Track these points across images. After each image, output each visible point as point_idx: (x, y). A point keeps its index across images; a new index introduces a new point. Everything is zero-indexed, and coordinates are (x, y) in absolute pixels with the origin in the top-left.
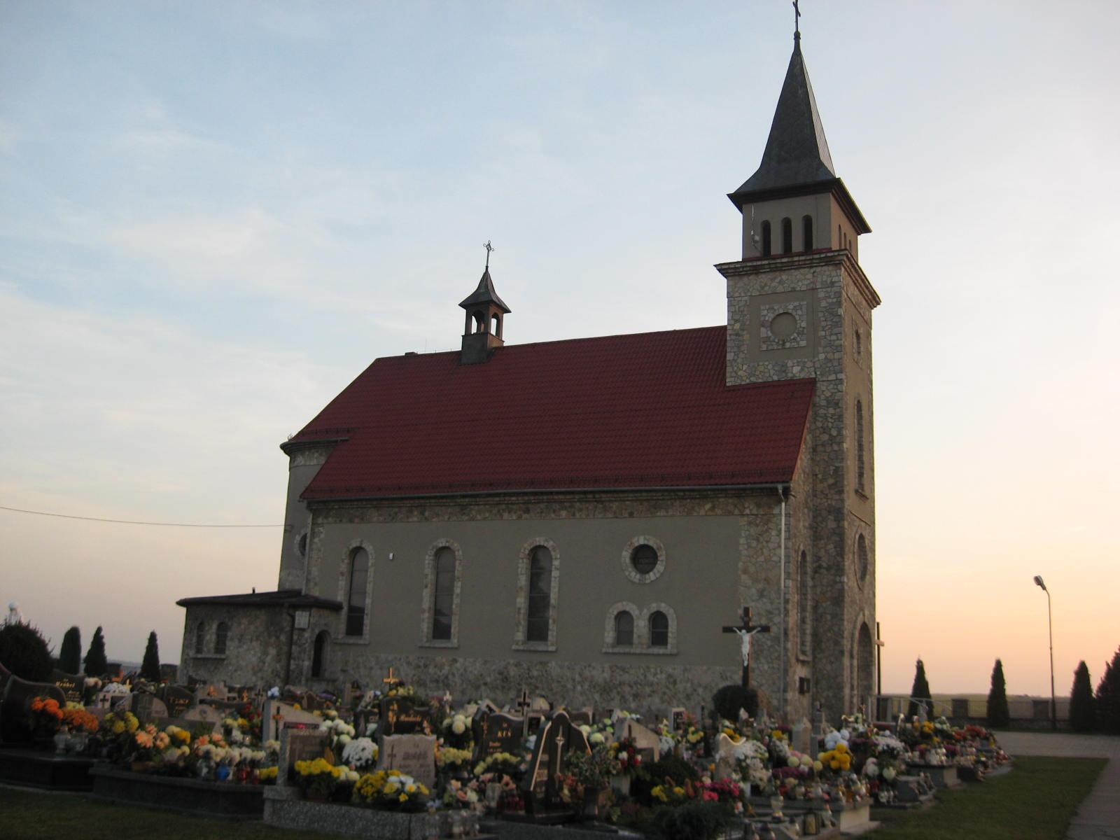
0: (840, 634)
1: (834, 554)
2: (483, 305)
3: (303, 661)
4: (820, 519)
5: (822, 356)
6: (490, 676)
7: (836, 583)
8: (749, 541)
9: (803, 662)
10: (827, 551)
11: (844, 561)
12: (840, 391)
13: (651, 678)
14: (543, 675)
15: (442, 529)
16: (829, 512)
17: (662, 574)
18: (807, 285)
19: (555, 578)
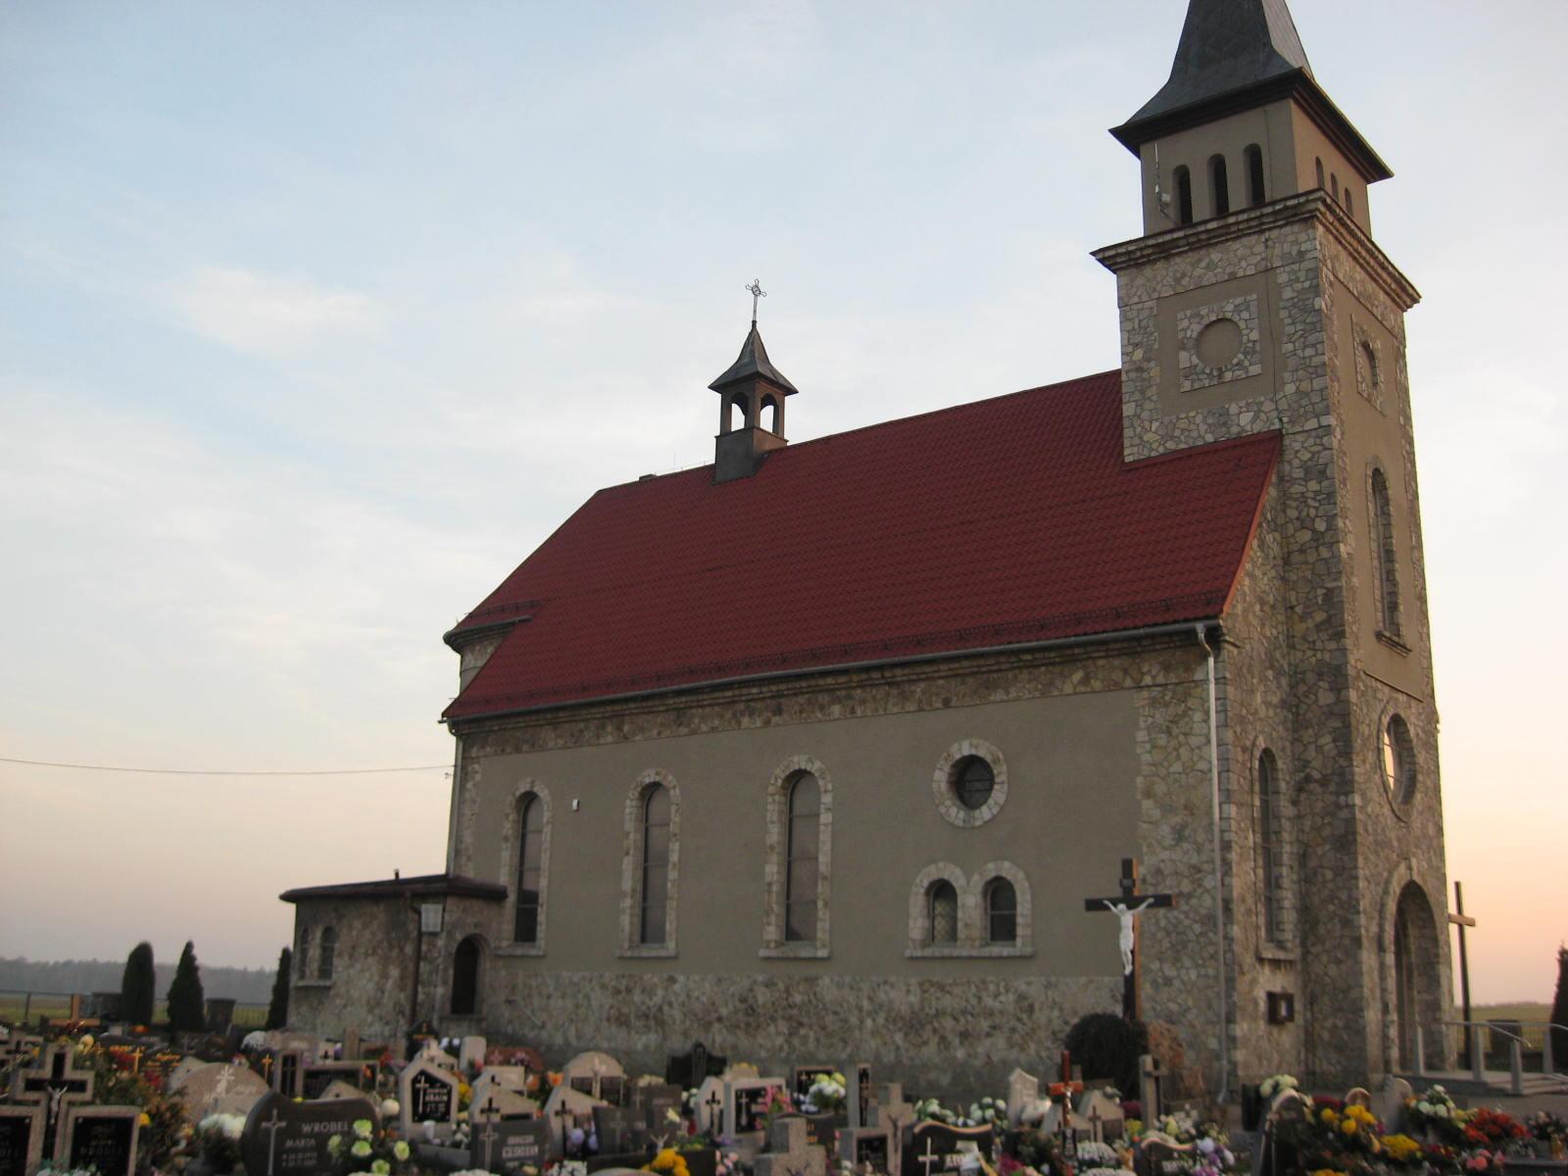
0: (1352, 905)
1: (1334, 752)
2: (750, 383)
3: (435, 987)
4: (1303, 688)
5: (1290, 388)
6: (727, 1005)
7: (1339, 807)
8: (1153, 736)
9: (1276, 963)
10: (1319, 749)
11: (1352, 765)
12: (1326, 449)
13: (989, 1001)
14: (810, 1001)
15: (649, 751)
16: (1320, 675)
17: (1002, 808)
18: (1256, 265)
19: (826, 825)
